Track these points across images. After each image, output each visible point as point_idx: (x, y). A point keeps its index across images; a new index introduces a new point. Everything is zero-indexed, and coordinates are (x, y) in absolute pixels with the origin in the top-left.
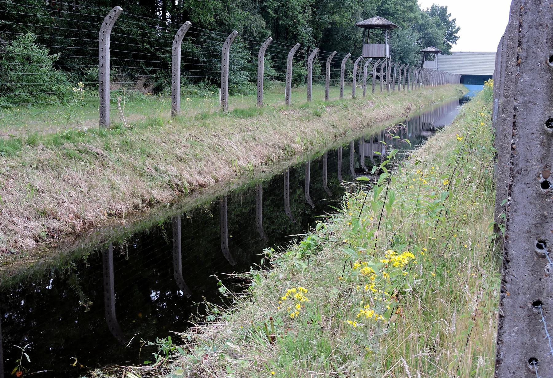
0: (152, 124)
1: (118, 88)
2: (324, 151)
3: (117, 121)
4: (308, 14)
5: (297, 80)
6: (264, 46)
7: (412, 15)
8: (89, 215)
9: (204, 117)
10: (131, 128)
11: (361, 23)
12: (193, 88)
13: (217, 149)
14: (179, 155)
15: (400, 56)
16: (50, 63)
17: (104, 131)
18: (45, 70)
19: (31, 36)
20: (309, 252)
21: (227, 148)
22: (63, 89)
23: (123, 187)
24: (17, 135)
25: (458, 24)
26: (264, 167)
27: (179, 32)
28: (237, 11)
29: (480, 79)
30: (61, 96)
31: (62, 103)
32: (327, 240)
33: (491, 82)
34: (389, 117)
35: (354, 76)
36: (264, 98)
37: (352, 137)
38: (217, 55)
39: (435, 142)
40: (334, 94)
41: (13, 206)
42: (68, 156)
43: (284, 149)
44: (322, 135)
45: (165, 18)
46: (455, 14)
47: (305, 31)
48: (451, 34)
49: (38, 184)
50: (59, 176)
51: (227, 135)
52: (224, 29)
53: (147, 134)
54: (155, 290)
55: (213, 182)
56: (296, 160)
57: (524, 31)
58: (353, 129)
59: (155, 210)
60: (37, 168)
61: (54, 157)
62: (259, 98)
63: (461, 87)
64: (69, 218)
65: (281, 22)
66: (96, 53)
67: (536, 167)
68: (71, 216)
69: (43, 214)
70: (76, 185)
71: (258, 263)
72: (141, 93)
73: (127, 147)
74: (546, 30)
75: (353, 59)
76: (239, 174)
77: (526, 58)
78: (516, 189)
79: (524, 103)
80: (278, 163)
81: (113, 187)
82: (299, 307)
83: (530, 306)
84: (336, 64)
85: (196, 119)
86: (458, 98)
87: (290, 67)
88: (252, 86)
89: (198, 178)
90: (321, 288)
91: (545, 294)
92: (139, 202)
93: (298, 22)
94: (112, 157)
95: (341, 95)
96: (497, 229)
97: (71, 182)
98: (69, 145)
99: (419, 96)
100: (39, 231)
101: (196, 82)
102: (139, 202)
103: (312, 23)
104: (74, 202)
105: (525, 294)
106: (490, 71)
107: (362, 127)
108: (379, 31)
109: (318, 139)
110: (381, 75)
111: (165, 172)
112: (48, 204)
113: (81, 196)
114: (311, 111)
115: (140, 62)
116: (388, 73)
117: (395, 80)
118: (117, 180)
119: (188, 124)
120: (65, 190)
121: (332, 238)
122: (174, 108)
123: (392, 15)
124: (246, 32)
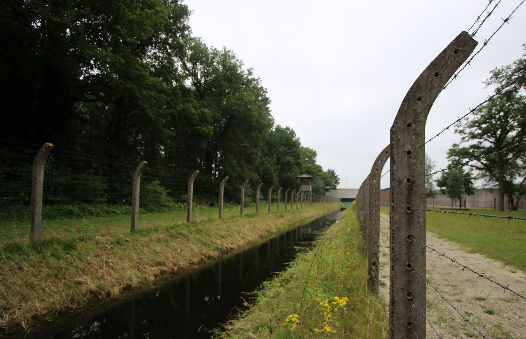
0: (210, 221)
1: (195, 204)
2: (285, 232)
3: (195, 219)
4: (277, 173)
5: (273, 200)
6: (259, 187)
7: (320, 173)
8: (181, 264)
9: (233, 217)
10: (201, 223)
11: (299, 176)
12: (228, 204)
13: (239, 232)
14: (222, 235)
15: (316, 190)
16: (165, 193)
17: (189, 224)
18: (163, 196)
19: (157, 182)
20: (283, 283)
21: (243, 232)
22: (170, 204)
23: (196, 250)
24: (149, 226)
25: (339, 177)
26: (259, 240)
27: (223, 181)
28: (247, 172)
29: (350, 200)
30: (169, 207)
31: (170, 211)
32: (291, 277)
33: (354, 202)
34: (312, 217)
35: (297, 199)
36: (259, 209)
37: (297, 225)
38: (239, 190)
39: (334, 228)
40: (289, 207)
41: (145, 260)
42: (172, 236)
43: (268, 231)
44: (284, 225)
45: (216, 174)
46: (337, 173)
47: (276, 180)
48: (336, 181)
49: (158, 250)
50: (167, 246)
51: (243, 226)
52: (242, 180)
53: (207, 225)
54: (207, 296)
55: (237, 247)
56: (273, 236)
57: (395, 196)
58: (297, 222)
59: (210, 261)
60: (158, 242)
61: (166, 236)
62: (257, 209)
63: (341, 203)
64: (171, 265)
65: (265, 176)
66: (187, 190)
67: (404, 257)
68: (172, 264)
69: (159, 264)
70: (175, 250)
71: (259, 287)
72: (205, 207)
73: (199, 231)
74: (405, 196)
75: (297, 192)
76: (249, 243)
77: (397, 208)
78: (396, 268)
79: (397, 228)
80: (265, 238)
81: (192, 250)
82: (294, 325)
83: (406, 325)
84: (289, 194)
85: (230, 218)
86: (340, 208)
87: (270, 196)
88: (253, 203)
89: (230, 245)
90: (292, 303)
91: (413, 319)
92: (203, 257)
93: (273, 176)
94: (192, 236)
95: (292, 207)
96: (370, 273)
97: (173, 248)
98: (173, 231)
99: (324, 207)
100: (157, 272)
101: (229, 202)
102: (203, 257)
103: (278, 177)
104: (174, 257)
105: (403, 319)
106: (354, 196)
107: (301, 221)
108: (307, 180)
109: (282, 227)
110: (308, 198)
111: (215, 243)
112: (162, 259)
113: (177, 255)
114: (279, 214)
115: (207, 194)
116: (311, 198)
117: (314, 201)
118: (194, 247)
119: (226, 221)
120: (170, 252)
121: (294, 276)
122: (220, 214)
123: (312, 173)
124: (251, 181)
